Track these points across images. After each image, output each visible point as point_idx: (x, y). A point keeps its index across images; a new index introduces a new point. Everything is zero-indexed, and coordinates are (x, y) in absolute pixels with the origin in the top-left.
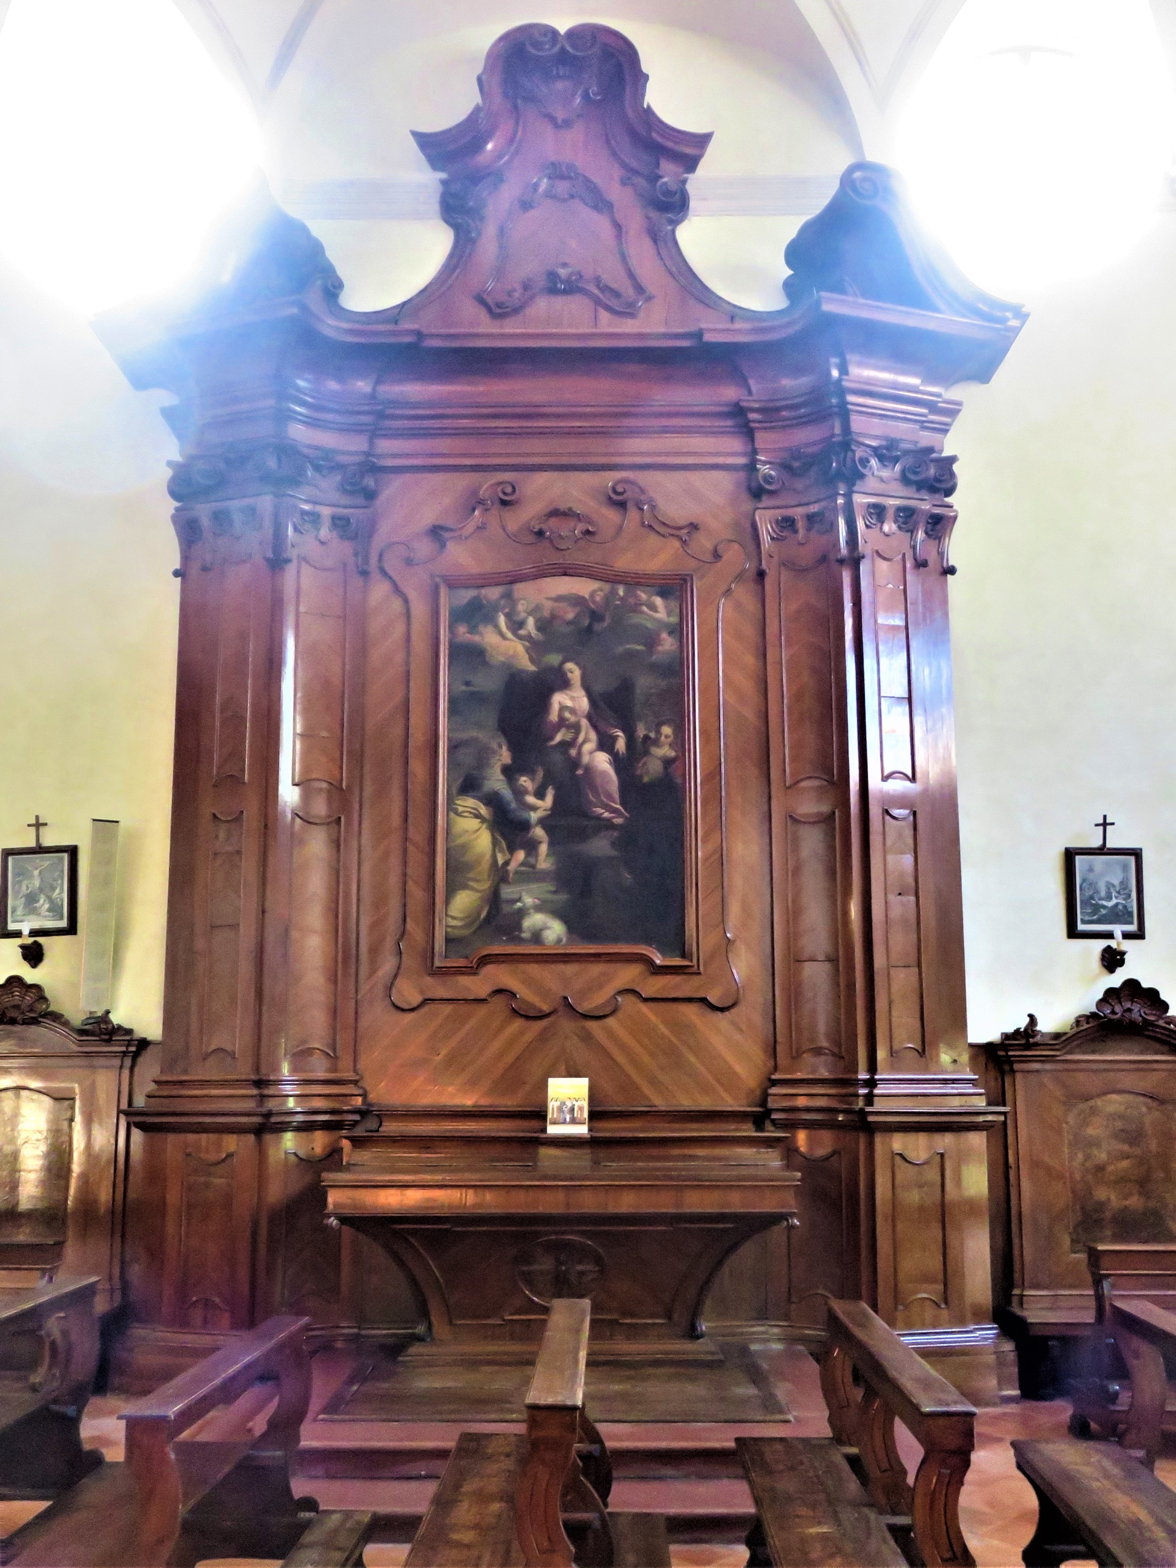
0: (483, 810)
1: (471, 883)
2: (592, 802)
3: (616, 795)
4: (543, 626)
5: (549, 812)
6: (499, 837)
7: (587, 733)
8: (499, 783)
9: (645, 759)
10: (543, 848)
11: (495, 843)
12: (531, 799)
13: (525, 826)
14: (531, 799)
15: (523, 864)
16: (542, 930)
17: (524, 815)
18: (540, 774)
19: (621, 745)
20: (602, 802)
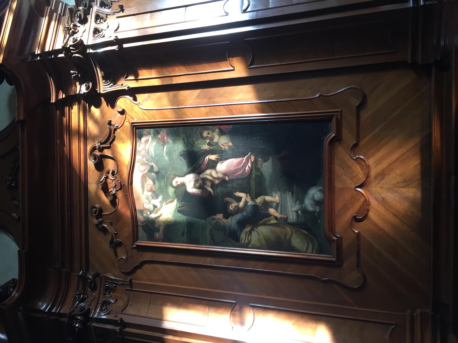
0: (248, 229)
1: (288, 237)
2: (243, 172)
3: (239, 159)
4: (156, 196)
5: (248, 194)
6: (262, 221)
7: (207, 175)
8: (233, 220)
9: (220, 144)
10: (268, 198)
11: (264, 224)
12: (241, 204)
13: (255, 207)
14: (241, 204)
15: (276, 209)
16: (314, 200)
17: (249, 209)
18: (228, 199)
19: (213, 157)
20: (243, 167)
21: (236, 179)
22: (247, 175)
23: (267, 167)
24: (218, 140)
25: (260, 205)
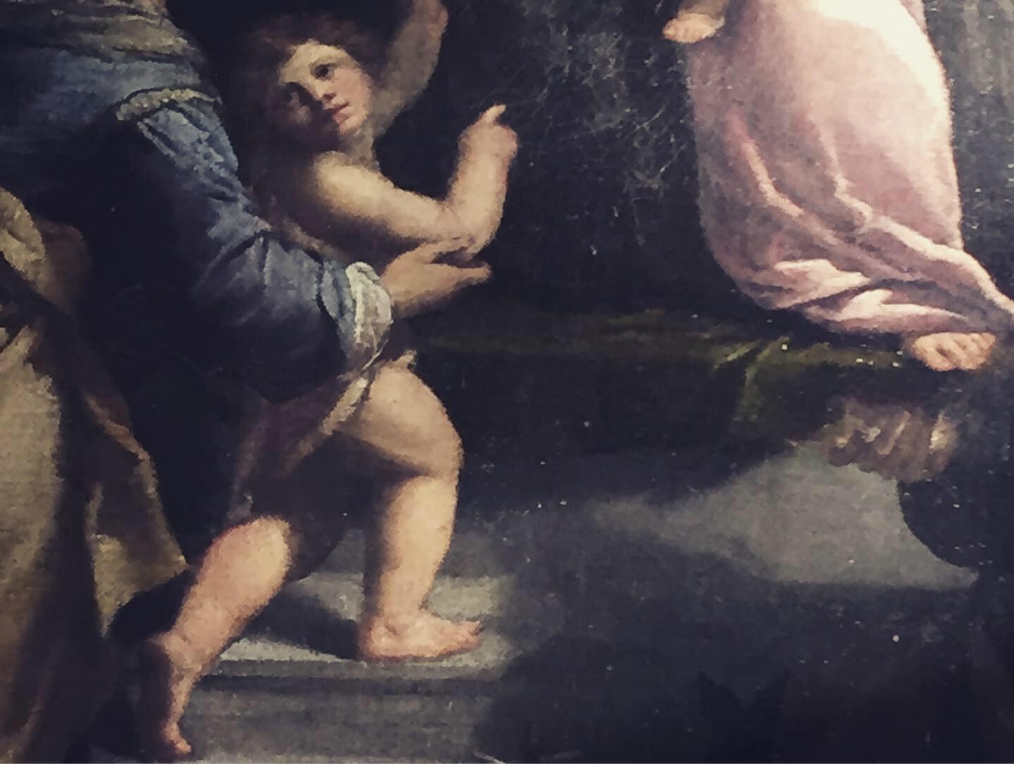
2: (770, 218)
3: (940, 189)
5: (480, 273)
10: (425, 517)
12: (353, 185)
13: (318, 356)
14: (353, 185)
15: (280, 616)
17: (286, 276)
18: (426, 28)
20: (845, 225)
21: (685, 133)
22: (733, 267)
23: (835, 521)
24: (987, 59)
25: (343, 409)
